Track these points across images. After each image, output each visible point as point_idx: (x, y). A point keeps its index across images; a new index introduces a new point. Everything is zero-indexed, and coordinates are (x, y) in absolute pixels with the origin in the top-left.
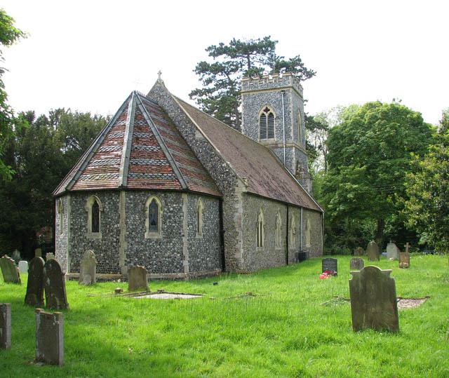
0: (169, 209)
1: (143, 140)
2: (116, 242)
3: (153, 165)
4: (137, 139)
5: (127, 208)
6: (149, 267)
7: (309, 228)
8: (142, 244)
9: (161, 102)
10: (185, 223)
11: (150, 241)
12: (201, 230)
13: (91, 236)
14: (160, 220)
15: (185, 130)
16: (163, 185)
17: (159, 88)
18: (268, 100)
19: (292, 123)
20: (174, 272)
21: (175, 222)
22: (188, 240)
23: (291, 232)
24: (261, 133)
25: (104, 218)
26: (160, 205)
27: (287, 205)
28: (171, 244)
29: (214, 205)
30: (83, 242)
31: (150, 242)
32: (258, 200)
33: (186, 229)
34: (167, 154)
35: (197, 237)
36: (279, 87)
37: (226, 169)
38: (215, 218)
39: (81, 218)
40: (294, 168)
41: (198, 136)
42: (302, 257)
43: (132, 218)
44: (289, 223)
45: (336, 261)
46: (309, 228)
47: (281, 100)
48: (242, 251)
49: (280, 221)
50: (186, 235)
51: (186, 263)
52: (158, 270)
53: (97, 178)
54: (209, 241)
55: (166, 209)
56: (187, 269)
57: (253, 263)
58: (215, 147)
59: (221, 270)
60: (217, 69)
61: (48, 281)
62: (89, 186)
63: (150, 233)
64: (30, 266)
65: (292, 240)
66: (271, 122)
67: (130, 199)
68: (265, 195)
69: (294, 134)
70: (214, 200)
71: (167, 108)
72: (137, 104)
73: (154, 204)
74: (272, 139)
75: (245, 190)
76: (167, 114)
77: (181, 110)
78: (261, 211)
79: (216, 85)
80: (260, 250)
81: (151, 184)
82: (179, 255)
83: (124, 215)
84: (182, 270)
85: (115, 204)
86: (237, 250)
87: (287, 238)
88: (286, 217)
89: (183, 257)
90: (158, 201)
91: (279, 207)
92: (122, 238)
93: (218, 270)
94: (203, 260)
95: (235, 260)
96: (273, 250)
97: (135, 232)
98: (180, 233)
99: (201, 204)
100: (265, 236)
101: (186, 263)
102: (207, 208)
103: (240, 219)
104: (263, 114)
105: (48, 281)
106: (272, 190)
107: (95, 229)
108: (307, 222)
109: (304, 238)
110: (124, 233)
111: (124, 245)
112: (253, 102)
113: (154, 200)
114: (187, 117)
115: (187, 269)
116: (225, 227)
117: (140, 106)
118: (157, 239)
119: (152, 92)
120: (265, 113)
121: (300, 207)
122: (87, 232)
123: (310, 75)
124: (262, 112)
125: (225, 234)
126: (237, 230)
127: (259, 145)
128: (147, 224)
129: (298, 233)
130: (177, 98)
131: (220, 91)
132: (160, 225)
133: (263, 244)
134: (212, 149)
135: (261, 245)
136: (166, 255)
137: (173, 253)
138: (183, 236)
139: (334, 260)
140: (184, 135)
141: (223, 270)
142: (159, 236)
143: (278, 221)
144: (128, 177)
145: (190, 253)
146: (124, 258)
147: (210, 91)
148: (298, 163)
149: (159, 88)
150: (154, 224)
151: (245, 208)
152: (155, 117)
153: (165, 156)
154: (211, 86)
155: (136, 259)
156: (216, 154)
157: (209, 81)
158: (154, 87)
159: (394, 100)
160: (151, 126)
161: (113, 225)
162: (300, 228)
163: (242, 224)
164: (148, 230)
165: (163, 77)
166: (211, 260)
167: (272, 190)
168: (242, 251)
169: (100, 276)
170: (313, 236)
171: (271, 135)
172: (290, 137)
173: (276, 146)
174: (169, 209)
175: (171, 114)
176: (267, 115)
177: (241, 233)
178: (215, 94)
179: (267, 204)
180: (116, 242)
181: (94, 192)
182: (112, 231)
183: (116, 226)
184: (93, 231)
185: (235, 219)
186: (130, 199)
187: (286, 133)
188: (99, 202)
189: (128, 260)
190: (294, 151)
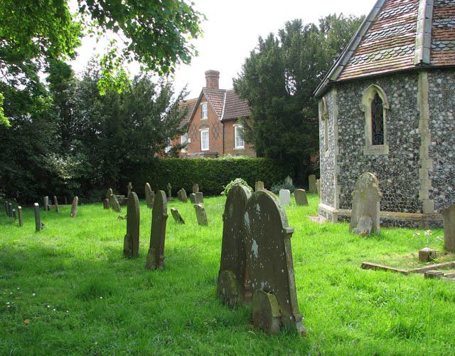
2: (414, 159)
5: (432, 101)
13: (371, 150)
25: (392, 121)
39: (354, 123)
43: (441, 118)
61: (255, 247)
67: (438, 85)
92: (424, 151)
105: (255, 247)
107: (378, 139)
110: (427, 143)
111: (428, 165)
155: (450, 188)
161: (408, 131)
180: (414, 159)
181: (372, 79)
183: (412, 132)
184: (374, 144)
186: (438, 85)
189: (436, 190)
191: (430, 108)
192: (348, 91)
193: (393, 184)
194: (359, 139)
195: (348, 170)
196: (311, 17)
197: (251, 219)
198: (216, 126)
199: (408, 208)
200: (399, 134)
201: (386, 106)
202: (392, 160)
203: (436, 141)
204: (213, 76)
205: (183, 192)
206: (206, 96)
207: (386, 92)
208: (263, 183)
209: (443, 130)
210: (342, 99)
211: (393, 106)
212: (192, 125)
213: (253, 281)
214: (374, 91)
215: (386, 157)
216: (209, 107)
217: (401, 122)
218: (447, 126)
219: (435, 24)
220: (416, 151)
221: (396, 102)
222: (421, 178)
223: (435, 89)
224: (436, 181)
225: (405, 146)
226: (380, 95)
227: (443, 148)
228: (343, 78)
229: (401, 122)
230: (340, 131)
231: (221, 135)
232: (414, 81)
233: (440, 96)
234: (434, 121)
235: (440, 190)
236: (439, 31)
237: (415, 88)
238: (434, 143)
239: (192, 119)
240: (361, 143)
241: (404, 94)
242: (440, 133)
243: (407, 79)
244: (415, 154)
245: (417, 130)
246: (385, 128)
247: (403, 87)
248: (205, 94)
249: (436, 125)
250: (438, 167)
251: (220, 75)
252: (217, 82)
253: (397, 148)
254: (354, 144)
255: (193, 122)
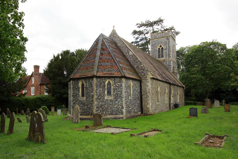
0: (116, 85)
1: (105, 54)
2: (92, 101)
3: (109, 66)
4: (102, 54)
5: (97, 85)
6: (107, 112)
7: (179, 93)
8: (104, 102)
9: (114, 39)
10: (123, 92)
11: (107, 100)
12: (131, 95)
13: (81, 98)
14: (112, 91)
15: (125, 51)
16: (113, 74)
17: (114, 33)
18: (161, 42)
19: (171, 51)
20: (119, 115)
21: (119, 91)
22: (125, 100)
23: (172, 95)
24: (158, 56)
25: (86, 90)
26: (112, 84)
27: (170, 84)
28: (117, 102)
29: (138, 84)
30: (78, 101)
31: (107, 101)
32: (158, 82)
33: (124, 94)
34: (116, 61)
35: (130, 98)
36: (165, 36)
37: (143, 67)
38: (138, 89)
39: (76, 91)
40: (172, 69)
41: (131, 53)
42: (176, 106)
43: (99, 90)
44: (171, 91)
45: (196, 109)
46: (179, 93)
47: (166, 42)
48: (150, 104)
49: (167, 91)
50: (124, 97)
51: (124, 110)
52: (111, 114)
53: (84, 72)
54: (135, 100)
55: (115, 85)
56: (125, 113)
57: (155, 110)
58: (138, 58)
59: (141, 113)
60: (141, 33)
61: (36, 125)
62: (80, 76)
63: (108, 97)
64: (10, 120)
65: (172, 99)
66: (162, 51)
67: (98, 81)
68: (160, 79)
69: (172, 56)
70: (138, 81)
71: (117, 42)
72: (103, 39)
73: (109, 83)
74: (163, 58)
75: (152, 77)
76: (117, 44)
77: (123, 42)
78: (159, 86)
79: (140, 40)
80: (158, 103)
81: (108, 74)
82: (121, 107)
83: (95, 89)
84: (122, 114)
85: (91, 84)
86: (148, 104)
87: (170, 98)
88: (169, 89)
89: (123, 108)
90: (111, 82)
91: (166, 85)
92: (94, 99)
93: (140, 113)
94: (132, 108)
95: (147, 108)
96: (164, 103)
97: (100, 97)
98: (121, 96)
99: (131, 83)
100: (161, 97)
101: (124, 110)
102: (135, 85)
103: (149, 90)
104: (159, 48)
105: (36, 125)
106: (163, 78)
107: (83, 95)
108: (178, 91)
109: (177, 99)
110: (95, 97)
111: (96, 103)
112: (155, 44)
113: (109, 81)
114: (126, 45)
115: (125, 113)
116: (143, 93)
117: (104, 40)
118: (111, 100)
119: (111, 35)
120: (160, 47)
121: (175, 85)
122: (79, 97)
123: (177, 33)
124: (159, 47)
125: (143, 97)
126: (148, 95)
127: (157, 60)
128: (106, 93)
129: (175, 96)
130: (124, 40)
131: (142, 42)
132: (112, 93)
133: (160, 101)
134: (137, 59)
135: (159, 102)
136: (115, 107)
137: (118, 106)
138: (123, 98)
139: (194, 108)
140: (124, 53)
141: (142, 113)
142: (111, 98)
143: (166, 91)
144: (97, 71)
145: (126, 105)
146: (95, 108)
147: (137, 42)
148: (173, 67)
149: (114, 33)
150: (109, 93)
151: (152, 85)
152: (111, 45)
153: (114, 61)
154: (138, 40)
155: (101, 109)
156: (139, 61)
157: (137, 38)
158: (111, 33)
159: (213, 40)
160: (109, 48)
161: (90, 93)
162: (175, 94)
163: (150, 92)
164: (106, 95)
165: (115, 28)
166: (136, 109)
167: (163, 78)
168: (150, 104)
169: (82, 117)
170: (180, 97)
171: (162, 57)
172: (171, 57)
173: (164, 61)
174: (116, 85)
175: (119, 45)
176: (161, 48)
177: (150, 96)
178: (140, 43)
179: (162, 83)
180: (92, 101)
181: (81, 78)
182: (90, 96)
183: (91, 94)
184: (82, 97)
185: (147, 90)
186: (98, 81)
187: (169, 55)
188: (84, 83)
189: (97, 109)
190: (172, 62)
191: (96, 87)
192: (75, 81)
193: (86, 108)
194: (78, 95)
195: (75, 104)
196: (73, 50)
197: (36, 119)
198: (37, 86)
199: (90, 115)
200: (88, 94)
201: (85, 86)
202: (86, 101)
203: (97, 96)
204: (37, 68)
205: (23, 111)
206: (34, 75)
207: (85, 82)
208: (54, 107)
209: (99, 93)
210: (74, 83)
211: (87, 86)
212: (28, 85)
213: (36, 133)
214: (82, 82)
215: (85, 100)
216: (35, 79)
217: (89, 91)
218: (100, 92)
219: (99, 64)
220: (92, 99)
221: (88, 85)
222: (93, 106)
223: (97, 82)
224: (97, 107)
225: (90, 97)
226: (84, 83)
227: (99, 98)
228: (74, 77)
229: (89, 91)
230: (73, 93)
231: (39, 90)
232: (92, 80)
233: (99, 84)
234: (97, 91)
235: (98, 109)
236: (100, 66)
237: (92, 82)
238: (97, 97)
239: (28, 83)
240: (78, 96)
241: (90, 83)
242: (98, 94)
243: (90, 79)
244: (92, 100)
245: (93, 93)
246: (85, 92)
247: (89, 81)
248: (33, 74)
249: (98, 92)
250: (98, 103)
251: (40, 67)
252: (39, 70)
253: (87, 98)
254: (77, 97)
255: (28, 84)
